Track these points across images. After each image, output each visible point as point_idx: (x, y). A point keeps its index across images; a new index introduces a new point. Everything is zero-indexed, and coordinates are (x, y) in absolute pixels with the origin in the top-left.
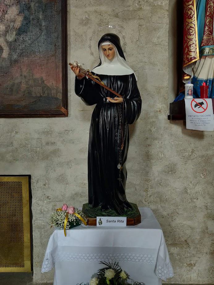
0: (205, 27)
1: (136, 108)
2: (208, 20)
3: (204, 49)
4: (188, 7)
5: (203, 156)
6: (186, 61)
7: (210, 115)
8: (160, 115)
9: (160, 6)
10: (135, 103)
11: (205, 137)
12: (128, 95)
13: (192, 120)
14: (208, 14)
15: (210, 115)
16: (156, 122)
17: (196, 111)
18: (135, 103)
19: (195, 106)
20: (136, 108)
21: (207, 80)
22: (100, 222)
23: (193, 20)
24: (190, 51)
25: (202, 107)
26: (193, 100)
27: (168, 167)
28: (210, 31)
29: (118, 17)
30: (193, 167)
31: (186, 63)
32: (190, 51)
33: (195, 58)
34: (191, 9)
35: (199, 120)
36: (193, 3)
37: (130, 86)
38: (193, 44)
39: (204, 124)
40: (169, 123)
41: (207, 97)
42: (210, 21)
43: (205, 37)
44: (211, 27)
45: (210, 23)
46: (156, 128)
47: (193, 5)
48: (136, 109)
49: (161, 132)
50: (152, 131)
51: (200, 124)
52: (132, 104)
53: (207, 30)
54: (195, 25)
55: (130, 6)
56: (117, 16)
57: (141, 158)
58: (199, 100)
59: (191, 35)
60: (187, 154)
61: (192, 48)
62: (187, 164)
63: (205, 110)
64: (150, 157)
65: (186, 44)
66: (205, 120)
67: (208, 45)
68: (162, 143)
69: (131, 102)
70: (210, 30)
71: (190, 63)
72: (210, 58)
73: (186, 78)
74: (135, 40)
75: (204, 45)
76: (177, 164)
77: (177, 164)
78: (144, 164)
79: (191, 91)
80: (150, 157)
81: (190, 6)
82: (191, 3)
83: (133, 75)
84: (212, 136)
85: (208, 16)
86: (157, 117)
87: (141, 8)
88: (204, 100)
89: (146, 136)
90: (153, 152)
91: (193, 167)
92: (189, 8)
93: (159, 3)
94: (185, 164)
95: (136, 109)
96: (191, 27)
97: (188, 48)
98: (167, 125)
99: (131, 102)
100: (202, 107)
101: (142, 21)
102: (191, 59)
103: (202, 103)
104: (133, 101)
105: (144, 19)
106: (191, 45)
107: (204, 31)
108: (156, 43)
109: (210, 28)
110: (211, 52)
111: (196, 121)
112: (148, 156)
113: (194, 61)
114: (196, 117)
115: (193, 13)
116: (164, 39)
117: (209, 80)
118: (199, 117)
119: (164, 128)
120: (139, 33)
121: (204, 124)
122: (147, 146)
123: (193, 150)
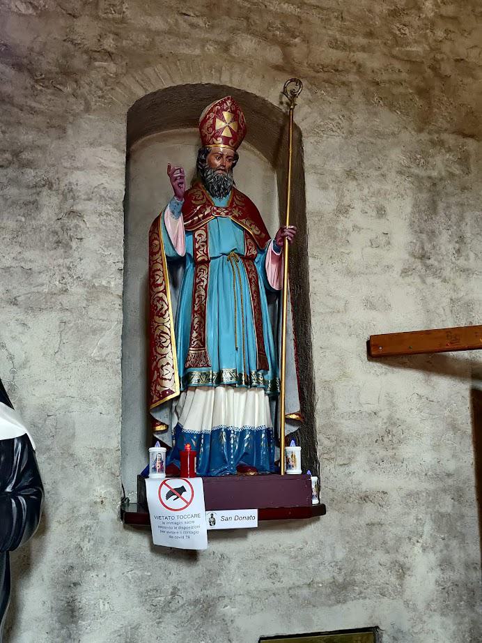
0: (191, 333)
1: (24, 514)
2: (196, 320)
3: (191, 374)
4: (156, 296)
5: (196, 602)
6: (156, 398)
7: (198, 516)
8: (102, 510)
9: (106, 287)
10: (23, 500)
11: (200, 557)
12: (10, 482)
13: (164, 525)
14: (196, 309)
15: (198, 516)
16: (93, 529)
17: (173, 508)
18: (23, 500)
19: (168, 496)
20: (24, 514)
21: (201, 434)
22: (212, 520)
23: (167, 319)
24: (163, 379)
25: (182, 498)
26: (164, 482)
27: (120, 636)
28: (200, 340)
29: (17, 305)
30: (175, 630)
31: (156, 401)
32: (163, 379)
33: (172, 392)
34: (161, 299)
35: (176, 526)
36: (165, 289)
37: (15, 458)
38: (168, 364)
39: (188, 535)
40: (122, 527)
41: (193, 475)
42: (200, 322)
43: (192, 352)
44: (202, 334)
45: (199, 325)
46: (92, 542)
47: (165, 293)
48: (24, 517)
49: (104, 551)
50: (84, 549)
51: (179, 535)
52: (14, 505)
53: (196, 337)
54: (169, 329)
55: (43, 285)
56: (14, 302)
57: (55, 618)
58: (176, 483)
59: (163, 347)
60: (163, 599)
61: (166, 372)
62: (163, 625)
63: (188, 504)
64: (76, 614)
65: (155, 363)
66: (189, 525)
67: (197, 366)
68: (105, 576)
69: (13, 501)
70: (199, 338)
71: (162, 402)
72: (204, 390)
73: (159, 428)
74: (51, 352)
75: (190, 366)
76: (140, 624)
77: (140, 624)
78: (64, 632)
79: (162, 463)
80: (76, 614)
81: (161, 295)
82: (161, 288)
83: (24, 439)
84: (214, 553)
85: (196, 312)
86: (94, 516)
87: (66, 290)
88: (187, 481)
89: (70, 561)
90: (84, 601)
91: (175, 630)
92: (158, 297)
93: (104, 283)
94: (159, 623)
95: (24, 517)
96: (163, 332)
97: (158, 372)
98: (118, 534)
99: (13, 501)
100: (182, 498)
101: (68, 314)
102: (164, 394)
103: (182, 490)
104: (20, 497)
105: (71, 311)
106: (163, 366)
107: (191, 340)
108: (97, 359)
109: (200, 334)
110: (204, 380)
111: (171, 528)
112: (73, 611)
113: (169, 398)
114: (171, 521)
115: (166, 307)
116: (113, 351)
117: (205, 434)
118: (176, 520)
119: (111, 540)
120: (61, 337)
121: (188, 535)
122: (72, 585)
123: (175, 588)
